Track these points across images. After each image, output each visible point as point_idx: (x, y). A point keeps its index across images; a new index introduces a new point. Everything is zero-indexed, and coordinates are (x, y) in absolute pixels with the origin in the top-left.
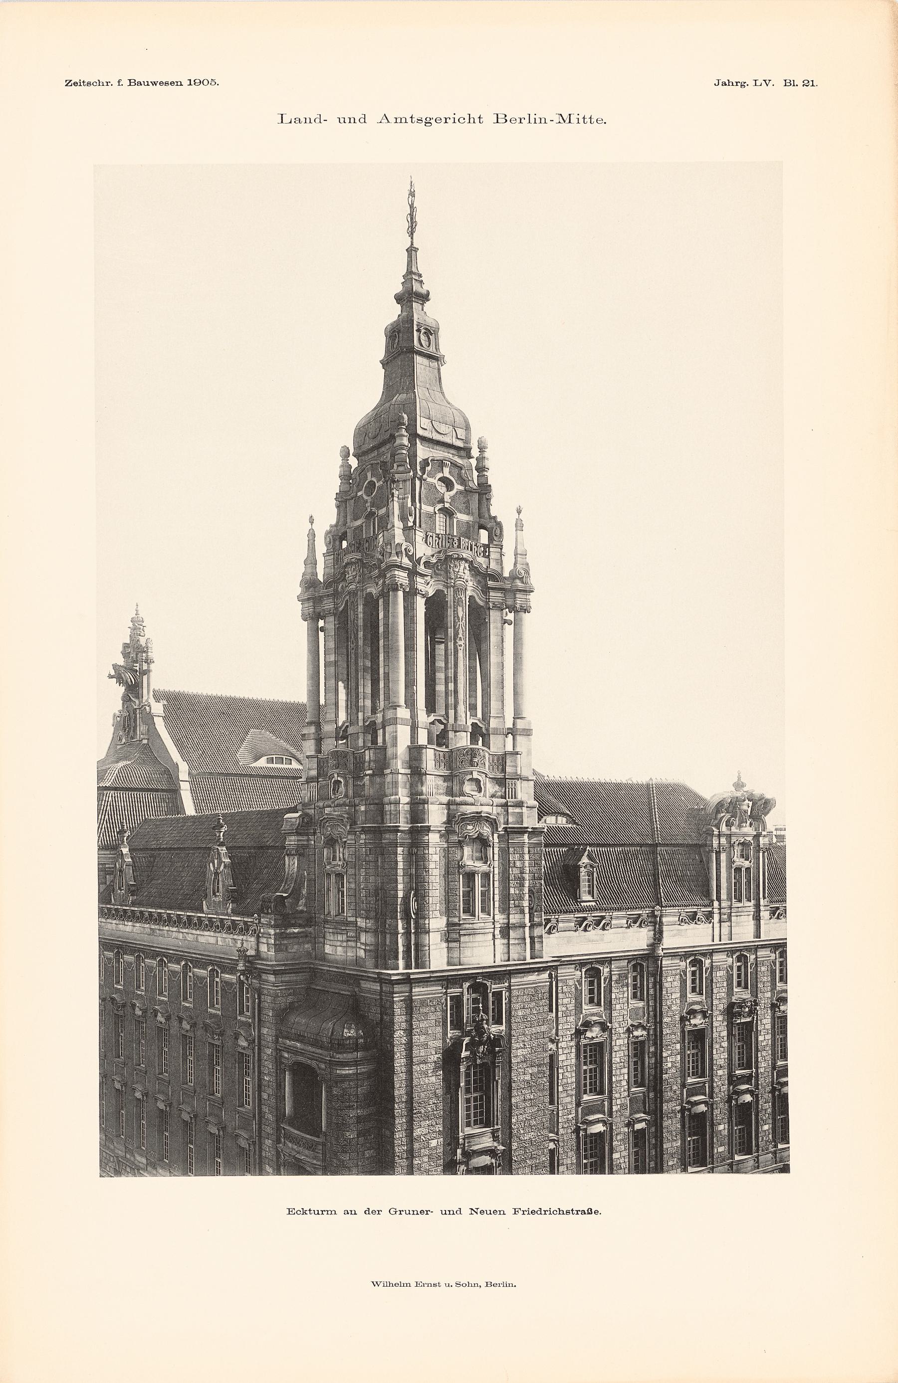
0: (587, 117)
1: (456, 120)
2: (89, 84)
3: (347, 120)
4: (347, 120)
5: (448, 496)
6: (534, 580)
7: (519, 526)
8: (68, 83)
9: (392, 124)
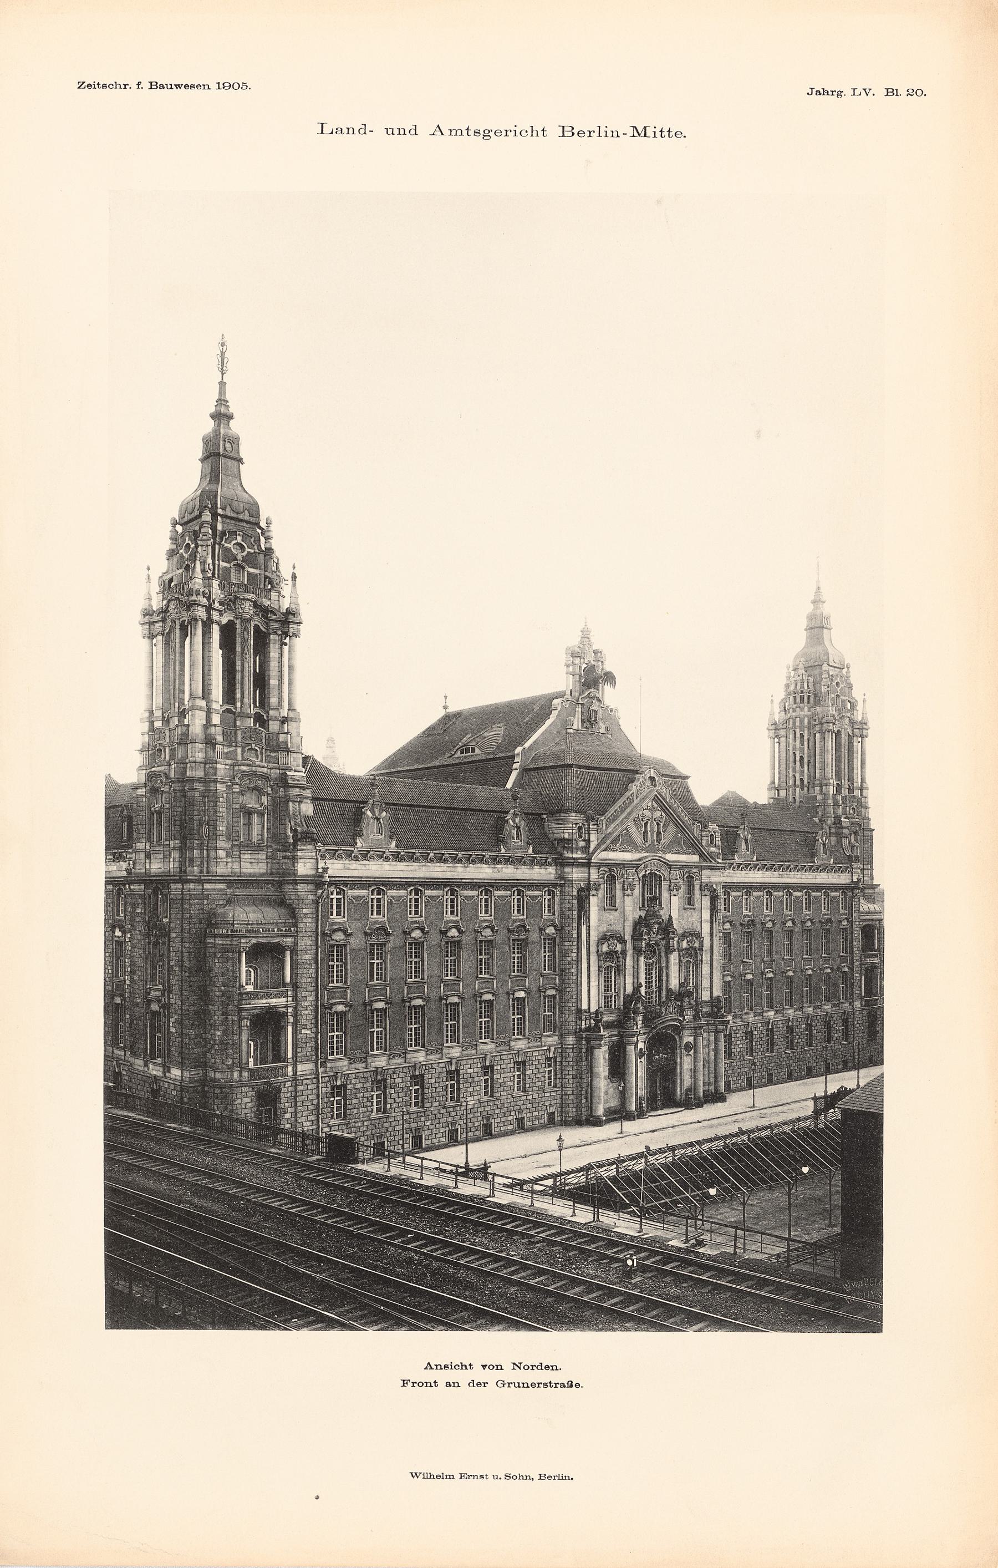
0: (665, 130)
1: (518, 133)
2: (104, 86)
3: (396, 132)
4: (396, 132)
5: (239, 557)
6: (870, 725)
7: (294, 577)
8: (81, 85)
9: (446, 138)
